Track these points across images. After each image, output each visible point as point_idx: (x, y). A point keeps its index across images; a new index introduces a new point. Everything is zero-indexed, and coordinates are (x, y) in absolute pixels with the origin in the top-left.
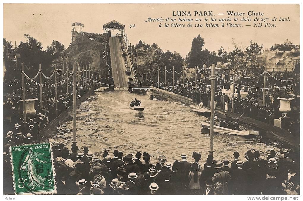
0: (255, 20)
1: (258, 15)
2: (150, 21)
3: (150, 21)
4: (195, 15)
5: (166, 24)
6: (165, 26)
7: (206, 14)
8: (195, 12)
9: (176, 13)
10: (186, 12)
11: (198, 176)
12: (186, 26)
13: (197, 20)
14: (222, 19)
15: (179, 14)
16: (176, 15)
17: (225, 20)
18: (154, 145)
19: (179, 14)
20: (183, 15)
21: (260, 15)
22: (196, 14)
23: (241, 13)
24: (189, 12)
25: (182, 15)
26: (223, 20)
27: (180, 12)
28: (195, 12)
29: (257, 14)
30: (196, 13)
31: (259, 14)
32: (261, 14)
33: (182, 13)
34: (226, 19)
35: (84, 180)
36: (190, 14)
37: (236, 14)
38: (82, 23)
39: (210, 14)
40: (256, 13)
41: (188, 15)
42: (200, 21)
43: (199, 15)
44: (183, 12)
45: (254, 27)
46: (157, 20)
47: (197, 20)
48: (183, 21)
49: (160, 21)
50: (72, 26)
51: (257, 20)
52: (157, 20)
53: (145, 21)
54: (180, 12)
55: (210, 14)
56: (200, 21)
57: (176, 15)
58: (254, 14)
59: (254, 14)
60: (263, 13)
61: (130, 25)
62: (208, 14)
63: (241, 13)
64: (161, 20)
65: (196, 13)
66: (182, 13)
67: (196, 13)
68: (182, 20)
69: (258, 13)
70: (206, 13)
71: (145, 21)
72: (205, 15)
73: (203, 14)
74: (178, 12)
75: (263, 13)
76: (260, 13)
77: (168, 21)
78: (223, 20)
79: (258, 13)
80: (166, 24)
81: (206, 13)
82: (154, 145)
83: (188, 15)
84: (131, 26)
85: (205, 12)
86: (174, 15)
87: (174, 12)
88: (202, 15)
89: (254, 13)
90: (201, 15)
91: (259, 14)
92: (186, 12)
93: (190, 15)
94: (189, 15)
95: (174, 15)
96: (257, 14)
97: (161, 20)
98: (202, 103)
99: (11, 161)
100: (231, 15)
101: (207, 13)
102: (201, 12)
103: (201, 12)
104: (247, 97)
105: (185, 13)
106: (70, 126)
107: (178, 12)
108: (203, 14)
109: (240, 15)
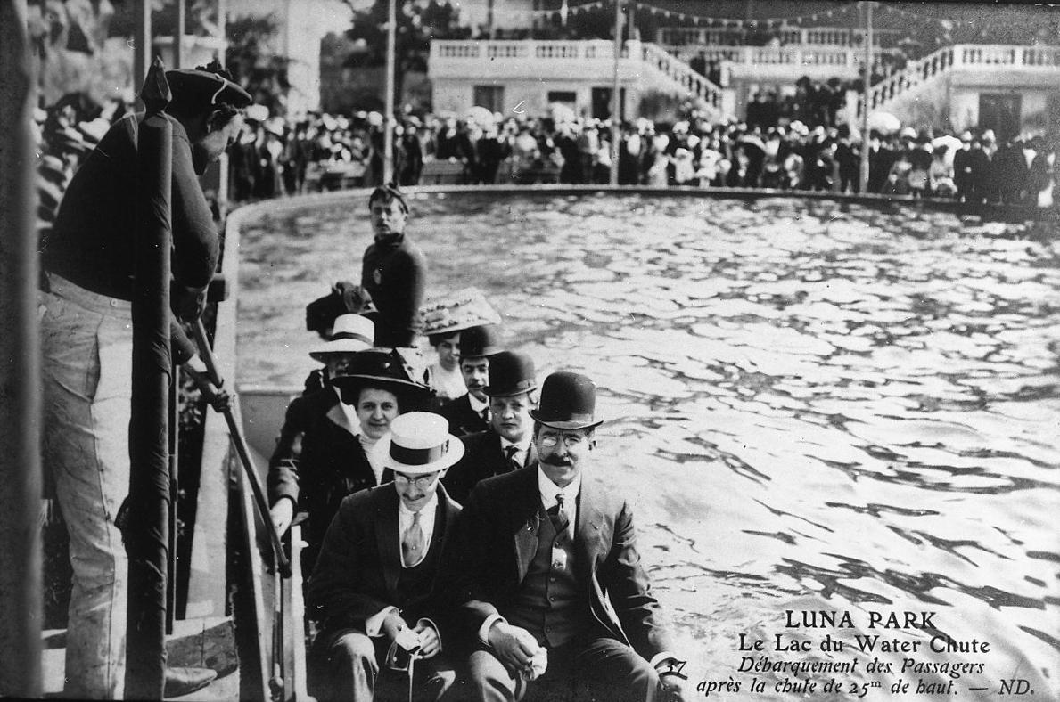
1: (967, 651)
4: (872, 626)
7: (912, 622)
8: (872, 614)
10: (834, 613)
11: (886, 183)
14: (707, 685)
15: (809, 622)
18: (674, 249)
19: (809, 622)
20: (823, 626)
21: (975, 651)
22: (872, 621)
23: (908, 644)
25: (818, 623)
26: (713, 686)
27: (814, 613)
29: (964, 648)
31: (971, 647)
32: (978, 647)
33: (819, 616)
34: (721, 684)
35: (295, 496)
36: (849, 621)
39: (910, 625)
41: (841, 626)
44: (824, 614)
45: (1002, 693)
54: (814, 613)
60: (987, 644)
63: (908, 644)
66: (819, 616)
70: (911, 617)
72: (906, 627)
73: (901, 622)
74: (805, 613)
75: (987, 644)
76: (975, 643)
78: (713, 686)
79: (967, 644)
81: (911, 617)
82: (674, 249)
85: (906, 614)
88: (897, 626)
91: (971, 647)
92: (834, 613)
96: (964, 648)
99: (495, 476)
100: (871, 648)
101: (915, 618)
102: (893, 614)
103: (893, 614)
105: (831, 616)
106: (526, 382)
107: (805, 613)
108: (901, 622)
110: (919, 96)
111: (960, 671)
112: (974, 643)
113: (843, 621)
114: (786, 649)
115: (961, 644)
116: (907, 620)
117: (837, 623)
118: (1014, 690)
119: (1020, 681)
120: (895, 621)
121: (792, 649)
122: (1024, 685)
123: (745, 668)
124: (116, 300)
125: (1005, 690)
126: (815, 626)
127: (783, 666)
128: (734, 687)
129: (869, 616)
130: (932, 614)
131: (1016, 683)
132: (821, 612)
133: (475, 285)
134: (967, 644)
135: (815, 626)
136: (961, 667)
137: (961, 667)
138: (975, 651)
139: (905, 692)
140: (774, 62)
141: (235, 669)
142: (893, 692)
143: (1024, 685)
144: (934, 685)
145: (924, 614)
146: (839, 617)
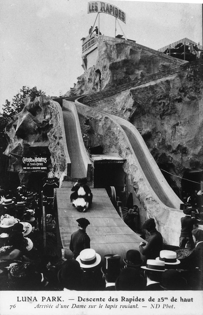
1: (25, 301)
2: (38, 307)
3: (38, 307)
6: (99, 307)
7: (54, 299)
8: (43, 297)
10: (31, 297)
12: (54, 307)
13: (91, 307)
15: (24, 300)
21: (101, 301)
22: (43, 299)
23: (95, 299)
24: (35, 297)
25: (27, 300)
26: (112, 306)
31: (191, 300)
32: (102, 300)
33: (27, 298)
36: (36, 299)
38: (120, 7)
39: (59, 300)
41: (33, 301)
42: (94, 307)
43: (47, 301)
46: (46, 307)
47: (91, 307)
48: (78, 307)
49: (49, 307)
50: (88, 13)
52: (46, 307)
53: (35, 308)
55: (59, 300)
56: (94, 307)
57: (21, 301)
58: (182, 300)
59: (182, 300)
61: (11, 306)
62: (56, 300)
63: (95, 299)
64: (50, 307)
65: (44, 298)
66: (27, 298)
67: (44, 298)
68: (78, 307)
70: (54, 298)
71: (35, 308)
72: (53, 301)
73: (51, 299)
74: (23, 297)
77: (58, 307)
79: (190, 299)
83: (33, 301)
84: (11, 306)
85: (53, 297)
86: (18, 301)
87: (19, 298)
88: (50, 301)
89: (183, 299)
91: (191, 300)
92: (31, 297)
93: (36, 301)
94: (35, 300)
95: (18, 301)
97: (50, 307)
101: (55, 298)
102: (35, 297)
103: (49, 297)
105: (30, 298)
108: (51, 299)
109: (103, 300)
110: (119, 156)
112: (101, 299)
113: (34, 299)
115: (188, 299)
116: (122, 299)
117: (32, 300)
120: (49, 299)
123: (73, 307)
125: (152, 307)
126: (25, 301)
127: (79, 306)
129: (42, 298)
130: (60, 297)
132: (28, 297)
133: (120, 61)
134: (190, 299)
138: (101, 301)
142: (56, 307)
144: (79, 306)
145: (58, 297)
146: (33, 299)
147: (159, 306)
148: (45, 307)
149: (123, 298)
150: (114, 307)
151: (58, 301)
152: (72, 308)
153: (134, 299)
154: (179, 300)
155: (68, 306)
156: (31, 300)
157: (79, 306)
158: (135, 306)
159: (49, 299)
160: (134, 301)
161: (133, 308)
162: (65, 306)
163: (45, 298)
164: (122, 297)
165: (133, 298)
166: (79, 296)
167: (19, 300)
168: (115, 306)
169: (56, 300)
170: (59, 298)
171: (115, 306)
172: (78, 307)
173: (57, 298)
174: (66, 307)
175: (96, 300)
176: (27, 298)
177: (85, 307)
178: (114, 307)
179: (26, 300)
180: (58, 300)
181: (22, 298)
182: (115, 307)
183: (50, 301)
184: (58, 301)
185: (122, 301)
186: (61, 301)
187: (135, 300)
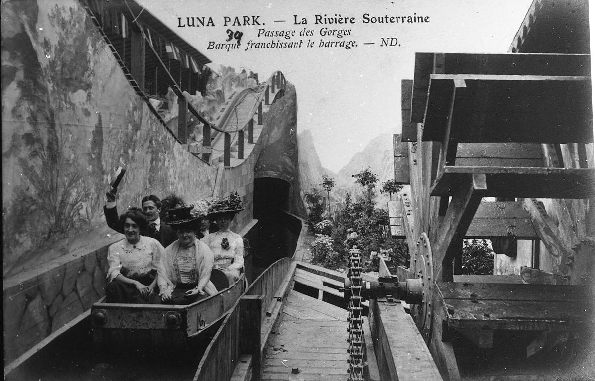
0: (302, 33)
5: (310, 40)
6: (308, 46)
7: (319, 20)
8: (225, 18)
9: (299, 20)
10: (204, 18)
15: (191, 23)
16: (184, 26)
17: (332, 32)
19: (191, 23)
20: (198, 26)
22: (226, 22)
23: (393, 18)
24: (211, 18)
25: (196, 24)
28: (225, 18)
30: (227, 20)
31: (384, 20)
32: (388, 20)
33: (195, 20)
36: (212, 22)
37: (411, 19)
39: (255, 23)
40: (379, 18)
41: (208, 25)
43: (234, 25)
45: (382, 45)
51: (305, 34)
53: (245, 50)
54: (193, 18)
55: (255, 23)
57: (184, 26)
62: (251, 22)
63: (393, 18)
65: (228, 20)
66: (195, 20)
67: (228, 20)
69: (382, 18)
70: (319, 18)
72: (244, 24)
73: (242, 22)
74: (188, 19)
75: (428, 18)
76: (386, 17)
79: (382, 18)
80: (310, 40)
81: (247, 19)
85: (244, 17)
86: (295, 23)
88: (239, 24)
90: (236, 24)
91: (384, 20)
92: (204, 18)
93: (213, 25)
95: (295, 23)
98: (586, 161)
101: (249, 19)
102: (237, 18)
103: (237, 18)
104: (514, 201)
105: (202, 20)
107: (188, 19)
108: (242, 22)
109: (351, 21)
111: (342, 34)
112: (386, 17)
114: (300, 23)
116: (245, 20)
117: (206, 24)
118: (389, 44)
119: (392, 39)
120: (238, 22)
121: (303, 23)
122: (394, 41)
124: (471, 226)
125: (384, 44)
126: (193, 26)
127: (261, 45)
128: (310, 33)
130: (258, 17)
131: (390, 40)
135: (193, 26)
136: (343, 32)
137: (343, 32)
139: (312, 46)
140: (195, 260)
141: (541, 203)
143: (394, 41)
145: (254, 17)
147: (397, 42)
148: (336, 46)
149: (247, 19)
150: (277, 47)
151: (254, 24)
152: (208, 49)
153: (336, 19)
154: (359, 19)
155: (314, 43)
156: (203, 24)
157: (261, 45)
158: (232, 48)
159: (210, 21)
160: (336, 23)
161: (294, 47)
162: (263, 45)
163: (230, 20)
164: (316, 16)
165: (415, 16)
166: (244, 16)
167: (181, 25)
168: (279, 45)
169: (251, 22)
170: (255, 19)
171: (279, 45)
172: (327, 44)
173: (251, 19)
174: (266, 46)
175: (395, 20)
176: (197, 20)
177: (312, 46)
178: (277, 47)
179: (195, 24)
180: (254, 23)
181: (187, 19)
182: (278, 46)
183: (239, 24)
184: (254, 24)
185: (317, 23)
186: (259, 24)
187: (377, 20)
